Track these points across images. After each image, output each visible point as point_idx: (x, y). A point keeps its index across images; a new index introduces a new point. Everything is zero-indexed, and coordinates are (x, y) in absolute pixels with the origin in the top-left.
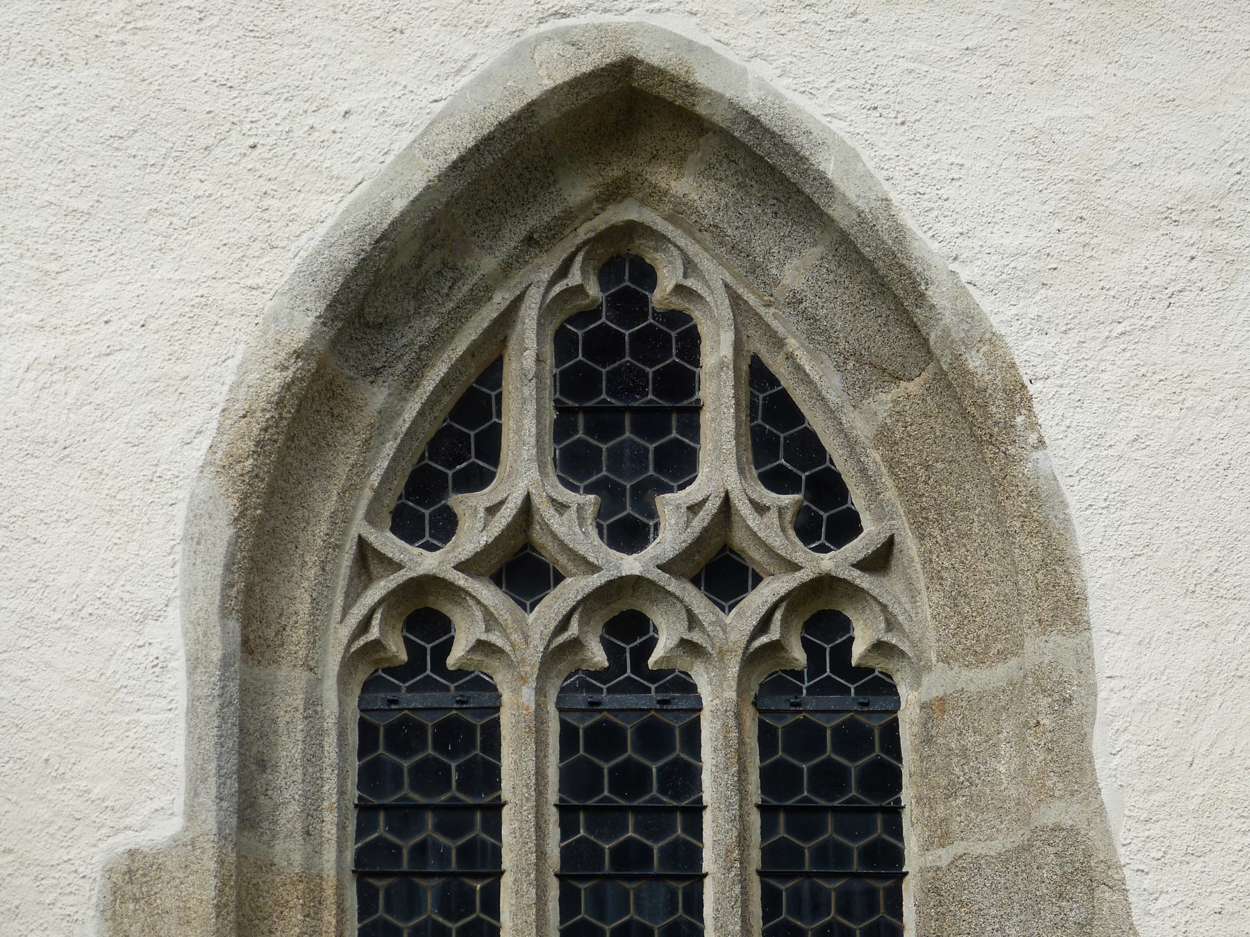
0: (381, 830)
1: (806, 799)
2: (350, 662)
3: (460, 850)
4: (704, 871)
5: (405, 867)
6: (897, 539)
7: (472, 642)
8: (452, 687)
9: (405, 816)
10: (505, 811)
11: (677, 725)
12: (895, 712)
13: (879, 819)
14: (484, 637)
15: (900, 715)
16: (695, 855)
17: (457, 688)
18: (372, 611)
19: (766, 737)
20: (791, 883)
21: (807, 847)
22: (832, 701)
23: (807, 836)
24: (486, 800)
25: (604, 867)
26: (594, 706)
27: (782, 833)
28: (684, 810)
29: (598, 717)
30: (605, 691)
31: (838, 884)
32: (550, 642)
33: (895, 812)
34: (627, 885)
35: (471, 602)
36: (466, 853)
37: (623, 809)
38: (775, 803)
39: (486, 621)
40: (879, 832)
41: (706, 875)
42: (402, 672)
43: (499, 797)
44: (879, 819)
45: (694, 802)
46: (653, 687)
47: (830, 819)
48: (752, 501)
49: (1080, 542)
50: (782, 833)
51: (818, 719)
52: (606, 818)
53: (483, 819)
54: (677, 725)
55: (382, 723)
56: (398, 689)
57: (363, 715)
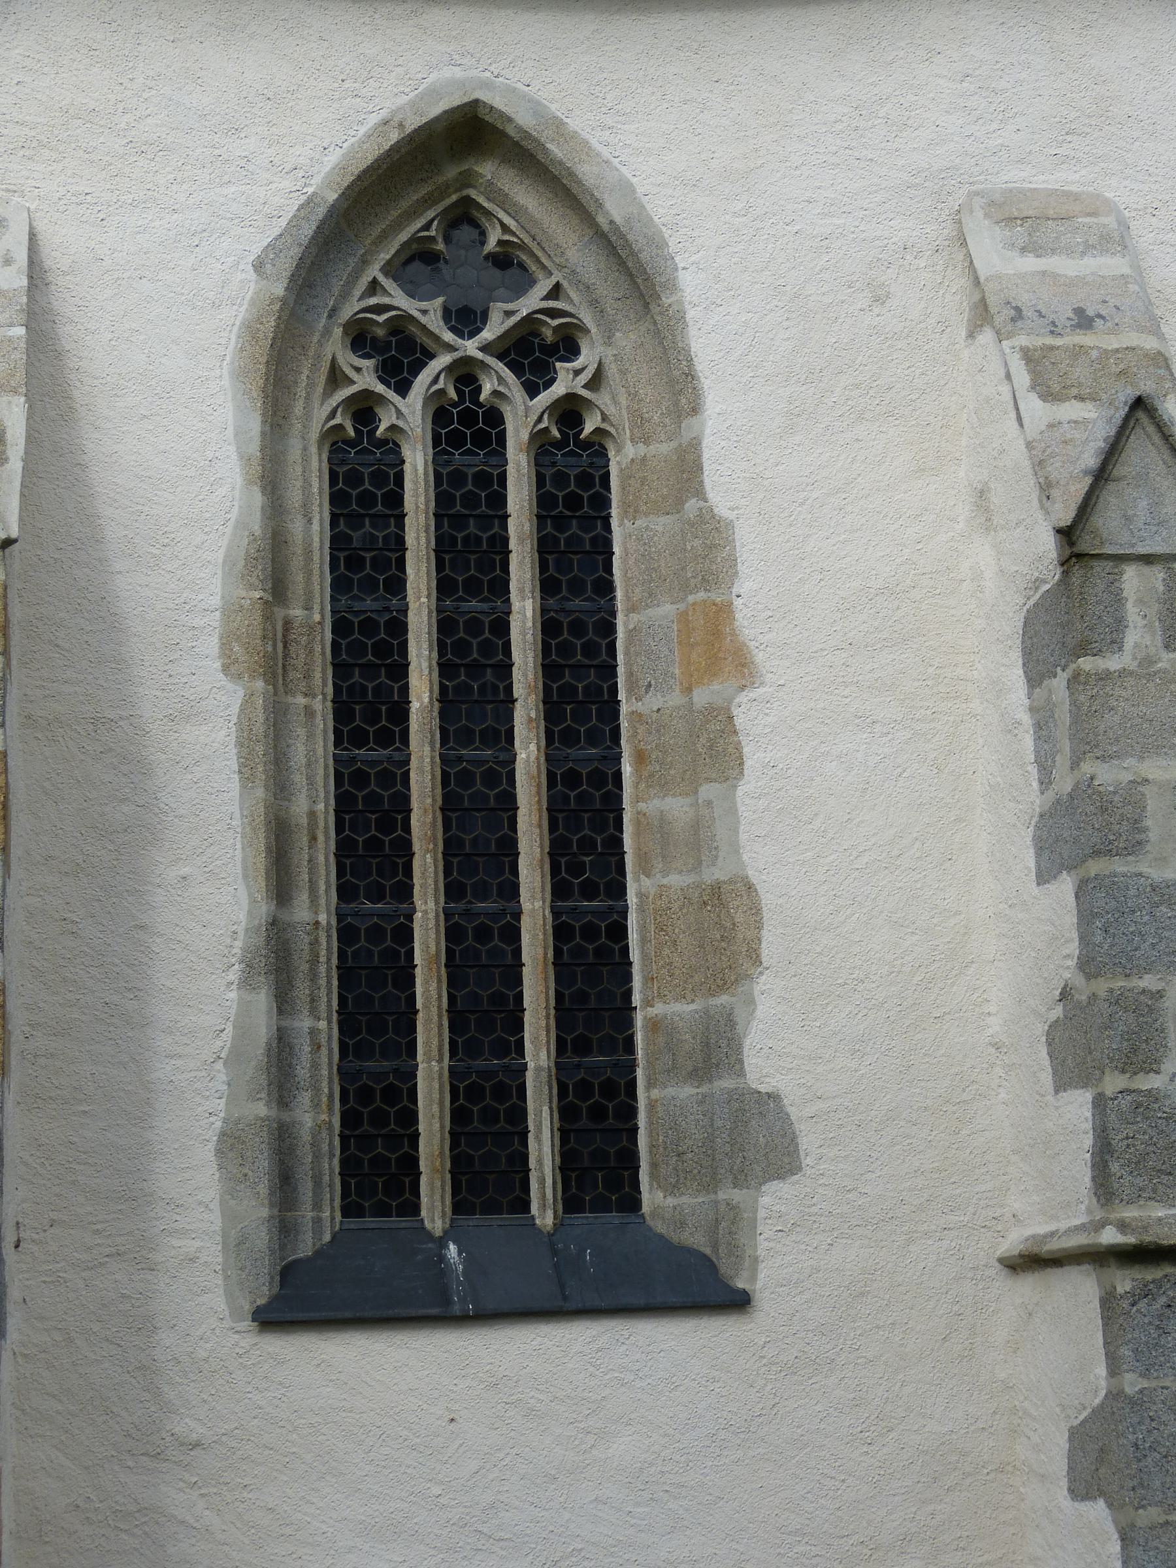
0: (342, 526)
1: (458, 511)
2: (324, 436)
3: (489, 539)
8: (353, 452)
9: (560, 523)
10: (509, 520)
13: (496, 522)
20: (372, 554)
22: (572, 460)
27: (549, 529)
35: (391, 406)
36: (594, 540)
38: (545, 514)
39: (397, 414)
44: (496, 522)
46: (353, 452)
47: (574, 522)
48: (351, 365)
49: (231, 408)
50: (549, 529)
51: (464, 469)
52: (355, 521)
53: (370, 522)
55: (342, 470)
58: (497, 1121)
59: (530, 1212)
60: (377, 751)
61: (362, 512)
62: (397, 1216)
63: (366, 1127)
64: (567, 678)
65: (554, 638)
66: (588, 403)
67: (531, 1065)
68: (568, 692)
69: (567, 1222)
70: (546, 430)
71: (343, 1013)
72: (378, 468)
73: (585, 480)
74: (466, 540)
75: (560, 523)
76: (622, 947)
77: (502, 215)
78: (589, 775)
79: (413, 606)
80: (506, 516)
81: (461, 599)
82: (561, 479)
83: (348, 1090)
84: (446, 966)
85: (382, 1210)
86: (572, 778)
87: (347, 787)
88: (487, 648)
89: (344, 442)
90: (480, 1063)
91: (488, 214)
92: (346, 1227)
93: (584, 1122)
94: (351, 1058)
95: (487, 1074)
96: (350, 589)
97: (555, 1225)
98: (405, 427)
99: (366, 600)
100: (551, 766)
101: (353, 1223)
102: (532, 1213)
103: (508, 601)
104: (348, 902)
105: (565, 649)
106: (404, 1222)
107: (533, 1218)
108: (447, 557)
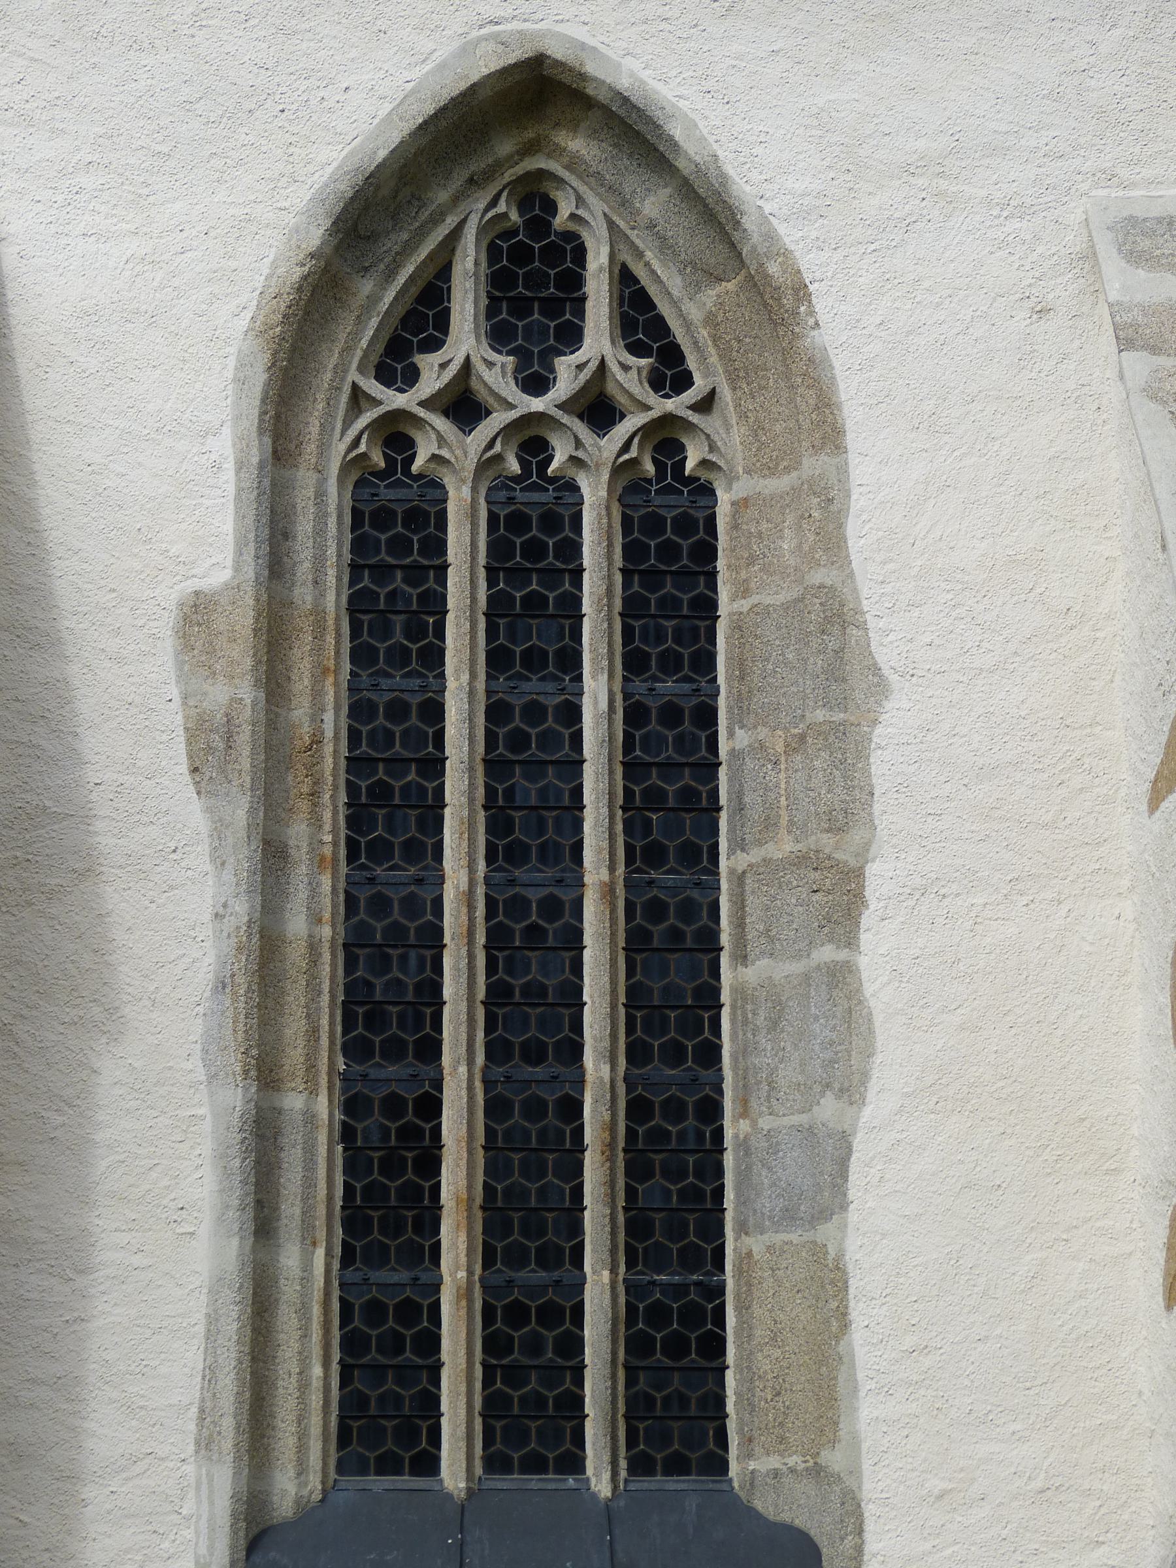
0: (366, 582)
1: (551, 564)
7: (429, 455)
13: (702, 579)
14: (437, 452)
15: (717, 509)
22: (671, 499)
28: (571, 571)
32: (345, 457)
33: (712, 575)
35: (428, 428)
38: (632, 567)
39: (439, 442)
42: (381, 475)
44: (702, 579)
46: (685, 491)
52: (518, 576)
54: (567, 514)
55: (367, 509)
58: (368, 1350)
59: (585, 1474)
60: (543, 872)
61: (529, 565)
62: (556, 1473)
63: (408, 1354)
64: (381, 774)
65: (638, 728)
66: (689, 427)
67: (447, 1278)
68: (654, 798)
69: (342, 1485)
70: (634, 462)
71: (632, 1209)
72: (685, 513)
73: (685, 524)
74: (527, 600)
75: (652, 579)
76: (576, 1128)
77: (575, 183)
78: (540, 902)
79: (451, 684)
80: (445, 567)
81: (655, 679)
82: (653, 524)
83: (495, 1308)
84: (625, 1150)
85: (535, 1465)
86: (656, 910)
87: (501, 918)
88: (414, 738)
89: (372, 474)
90: (522, 1275)
91: (561, 181)
92: (632, 1487)
93: (373, 1356)
94: (533, 1266)
95: (533, 1291)
96: (511, 665)
97: (469, 1489)
98: (721, 463)
99: (394, 677)
100: (491, 890)
101: (354, 1482)
102: (730, 1474)
103: (579, 678)
104: (637, 1067)
105: (518, 741)
106: (707, 1482)
107: (588, 1479)
108: (501, 621)
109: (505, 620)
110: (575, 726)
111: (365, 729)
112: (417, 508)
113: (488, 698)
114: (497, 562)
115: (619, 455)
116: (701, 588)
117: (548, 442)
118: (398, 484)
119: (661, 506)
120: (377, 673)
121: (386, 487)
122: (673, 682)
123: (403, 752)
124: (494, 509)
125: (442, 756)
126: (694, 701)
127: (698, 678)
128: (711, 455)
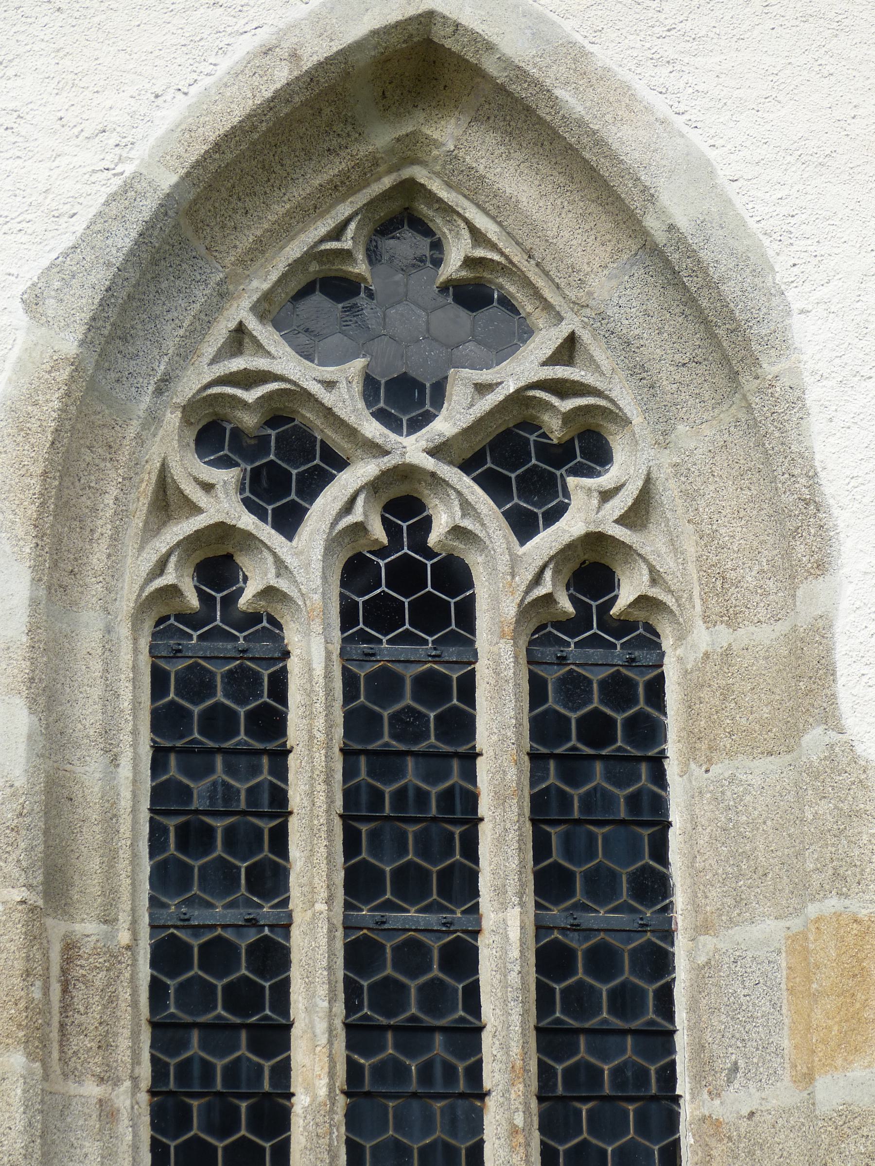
0: (173, 771)
2: (144, 605)
4: (480, 815)
5: (576, 815)
6: (653, 476)
7: (261, 587)
8: (195, 635)
10: (480, 762)
11: (641, 681)
12: (661, 666)
13: (455, 764)
14: (273, 582)
15: (477, 666)
16: (472, 799)
17: (201, 637)
18: (169, 554)
19: (350, 681)
21: (621, 794)
22: (596, 654)
23: (575, 783)
24: (462, 749)
25: (430, 808)
26: (562, 660)
28: (272, 754)
29: (568, 668)
30: (619, 647)
31: (650, 831)
32: (142, 589)
33: (657, 764)
34: (640, 830)
36: (634, 801)
37: (212, 752)
40: (265, 775)
41: (482, 819)
42: (191, 620)
43: (474, 747)
44: (644, 768)
45: (470, 749)
46: (618, 643)
51: (398, 668)
54: (641, 681)
55: (174, 668)
56: (568, 644)
57: (531, 667)
66: (626, 549)
70: (548, 599)
80: (472, 756)
81: (389, 906)
96: (570, 892)
109: (650, 831)
110: (278, 975)
111: (172, 983)
112: (431, 672)
113: (538, 938)
114: (545, 745)
115: (527, 592)
116: (455, 778)
117: (238, 567)
118: (216, 634)
119: (392, 661)
120: (189, 902)
121: (389, 642)
122: (370, 910)
123: (180, 1014)
124: (539, 671)
125: (284, 1022)
126: (252, 936)
127: (361, 906)
128: (653, 590)
